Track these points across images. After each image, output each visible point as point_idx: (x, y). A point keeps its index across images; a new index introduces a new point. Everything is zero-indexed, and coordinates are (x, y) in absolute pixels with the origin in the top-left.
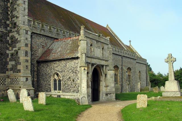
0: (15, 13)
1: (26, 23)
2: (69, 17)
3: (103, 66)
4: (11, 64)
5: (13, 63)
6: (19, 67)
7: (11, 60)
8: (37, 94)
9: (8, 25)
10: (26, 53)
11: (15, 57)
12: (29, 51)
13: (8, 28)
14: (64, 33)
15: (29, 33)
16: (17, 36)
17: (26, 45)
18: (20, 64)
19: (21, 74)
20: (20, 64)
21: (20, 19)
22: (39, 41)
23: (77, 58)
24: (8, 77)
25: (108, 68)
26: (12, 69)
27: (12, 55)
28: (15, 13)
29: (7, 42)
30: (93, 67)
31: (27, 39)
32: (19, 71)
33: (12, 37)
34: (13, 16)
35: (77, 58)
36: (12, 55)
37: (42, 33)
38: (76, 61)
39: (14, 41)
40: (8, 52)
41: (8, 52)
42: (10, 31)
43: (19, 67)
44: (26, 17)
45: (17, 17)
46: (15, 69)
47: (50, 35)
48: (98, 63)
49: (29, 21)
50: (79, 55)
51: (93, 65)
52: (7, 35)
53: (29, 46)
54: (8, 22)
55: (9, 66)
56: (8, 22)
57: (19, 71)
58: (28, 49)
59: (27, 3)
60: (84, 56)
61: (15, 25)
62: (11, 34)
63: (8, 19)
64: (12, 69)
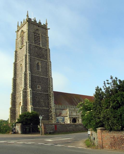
0: (51, 103)
1: (54, 106)
2: (72, 97)
3: (77, 118)
4: (51, 118)
5: (51, 117)
6: (53, 119)
7: (50, 117)
8: (13, 93)
9: (49, 107)
10: (54, 115)
11: (51, 116)
12: (55, 114)
13: (49, 108)
14: (67, 106)
15: (55, 109)
16: (51, 110)
17: (54, 113)
18: (53, 118)
19: (53, 121)
20: (53, 118)
21: (52, 105)
22: (58, 111)
23: (67, 116)
24: (50, 121)
25: (79, 118)
26: (51, 119)
27: (51, 115)
28: (51, 103)
29: (49, 112)
30: (73, 119)
31: (54, 111)
32: (53, 120)
33: (50, 110)
34: (50, 104)
35: (67, 116)
36: (51, 115)
37: (59, 108)
38: (67, 117)
39: (51, 112)
40: (49, 114)
41: (49, 114)
42: (50, 109)
43: (53, 119)
44: (54, 105)
45: (51, 105)
46: (52, 119)
47: (61, 108)
48: (75, 117)
49: (55, 105)
50: (68, 115)
51: (72, 118)
52: (49, 110)
53: (55, 113)
54: (49, 106)
55: (50, 118)
56: (49, 106)
57: (53, 120)
58: (55, 114)
59: (53, 97)
60: (68, 116)
61: (51, 107)
62: (50, 109)
63: (49, 105)
64: (51, 119)
